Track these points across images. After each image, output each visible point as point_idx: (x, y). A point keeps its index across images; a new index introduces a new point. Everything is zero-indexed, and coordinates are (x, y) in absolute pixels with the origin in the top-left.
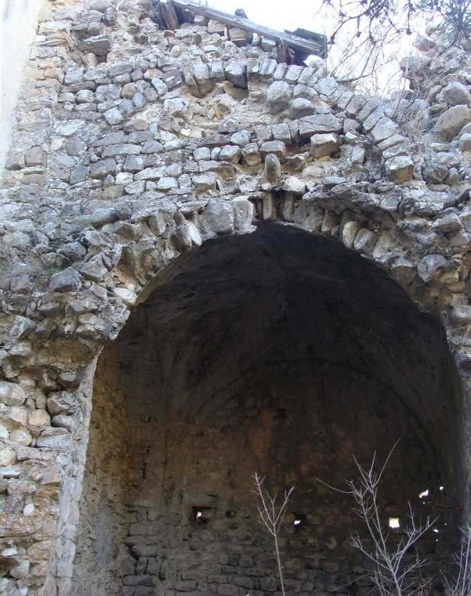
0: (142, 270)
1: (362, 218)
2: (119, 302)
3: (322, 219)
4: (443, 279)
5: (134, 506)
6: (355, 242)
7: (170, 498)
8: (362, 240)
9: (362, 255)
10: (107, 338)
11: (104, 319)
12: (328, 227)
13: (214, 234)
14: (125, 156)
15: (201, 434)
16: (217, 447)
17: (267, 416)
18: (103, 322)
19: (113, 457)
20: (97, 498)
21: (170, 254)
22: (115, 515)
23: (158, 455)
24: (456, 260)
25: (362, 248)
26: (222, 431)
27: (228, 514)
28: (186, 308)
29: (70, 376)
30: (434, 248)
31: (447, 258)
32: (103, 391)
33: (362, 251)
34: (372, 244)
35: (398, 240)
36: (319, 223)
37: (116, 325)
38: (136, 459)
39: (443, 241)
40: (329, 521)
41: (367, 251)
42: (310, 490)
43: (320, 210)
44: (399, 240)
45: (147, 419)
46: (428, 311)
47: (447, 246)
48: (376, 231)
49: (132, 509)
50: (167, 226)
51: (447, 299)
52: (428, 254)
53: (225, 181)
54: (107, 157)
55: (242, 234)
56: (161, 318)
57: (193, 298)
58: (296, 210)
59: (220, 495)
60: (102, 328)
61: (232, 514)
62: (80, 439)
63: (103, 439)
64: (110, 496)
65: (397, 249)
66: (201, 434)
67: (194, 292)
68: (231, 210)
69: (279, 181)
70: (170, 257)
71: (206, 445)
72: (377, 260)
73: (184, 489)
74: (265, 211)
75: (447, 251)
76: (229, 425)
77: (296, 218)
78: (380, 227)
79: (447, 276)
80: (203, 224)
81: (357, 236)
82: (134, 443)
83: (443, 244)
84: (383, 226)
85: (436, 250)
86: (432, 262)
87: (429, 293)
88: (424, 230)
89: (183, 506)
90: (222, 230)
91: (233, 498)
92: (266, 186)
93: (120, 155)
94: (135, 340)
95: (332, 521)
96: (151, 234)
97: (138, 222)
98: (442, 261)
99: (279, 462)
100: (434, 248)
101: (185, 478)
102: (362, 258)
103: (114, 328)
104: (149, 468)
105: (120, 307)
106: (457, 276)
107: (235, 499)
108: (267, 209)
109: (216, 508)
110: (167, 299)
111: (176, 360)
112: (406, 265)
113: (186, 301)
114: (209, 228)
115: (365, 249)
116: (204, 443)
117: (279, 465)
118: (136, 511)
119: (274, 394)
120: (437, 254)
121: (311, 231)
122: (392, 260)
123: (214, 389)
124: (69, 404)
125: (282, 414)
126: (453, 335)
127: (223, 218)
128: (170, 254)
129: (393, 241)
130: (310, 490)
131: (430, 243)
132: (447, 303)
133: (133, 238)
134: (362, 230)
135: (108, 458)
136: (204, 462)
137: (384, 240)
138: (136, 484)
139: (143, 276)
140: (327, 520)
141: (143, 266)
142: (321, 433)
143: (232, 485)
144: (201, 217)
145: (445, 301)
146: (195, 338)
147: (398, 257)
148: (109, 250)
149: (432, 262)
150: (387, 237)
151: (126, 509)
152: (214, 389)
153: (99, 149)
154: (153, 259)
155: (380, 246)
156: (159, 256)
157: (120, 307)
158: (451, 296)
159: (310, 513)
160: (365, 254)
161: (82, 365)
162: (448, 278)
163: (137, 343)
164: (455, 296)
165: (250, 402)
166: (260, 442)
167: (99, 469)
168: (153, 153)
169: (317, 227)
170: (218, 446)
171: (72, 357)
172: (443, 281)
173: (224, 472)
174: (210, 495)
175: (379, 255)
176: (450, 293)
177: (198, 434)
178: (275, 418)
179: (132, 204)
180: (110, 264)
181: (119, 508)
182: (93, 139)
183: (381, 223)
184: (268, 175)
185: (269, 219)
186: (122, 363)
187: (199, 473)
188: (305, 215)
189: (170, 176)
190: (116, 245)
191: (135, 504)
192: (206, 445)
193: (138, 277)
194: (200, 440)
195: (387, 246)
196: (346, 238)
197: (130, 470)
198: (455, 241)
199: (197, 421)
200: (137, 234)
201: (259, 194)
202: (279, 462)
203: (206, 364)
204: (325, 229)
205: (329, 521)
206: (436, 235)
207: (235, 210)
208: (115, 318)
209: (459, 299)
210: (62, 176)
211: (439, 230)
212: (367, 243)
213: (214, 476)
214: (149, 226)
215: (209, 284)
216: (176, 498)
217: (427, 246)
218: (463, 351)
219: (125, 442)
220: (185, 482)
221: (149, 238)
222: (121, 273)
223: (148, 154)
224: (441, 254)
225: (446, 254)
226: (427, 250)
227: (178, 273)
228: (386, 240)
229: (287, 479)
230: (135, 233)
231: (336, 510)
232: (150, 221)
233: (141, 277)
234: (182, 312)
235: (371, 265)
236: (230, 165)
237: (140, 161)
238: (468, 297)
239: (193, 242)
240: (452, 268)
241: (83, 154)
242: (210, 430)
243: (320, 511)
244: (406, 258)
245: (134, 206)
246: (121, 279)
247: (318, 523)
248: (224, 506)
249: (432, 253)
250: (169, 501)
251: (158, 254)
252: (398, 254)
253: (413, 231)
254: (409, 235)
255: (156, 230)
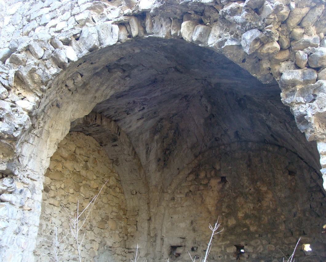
0: (36, 85)
1: (196, 17)
2: (20, 110)
3: (170, 26)
4: (265, 50)
5: (131, 249)
6: (193, 36)
7: (155, 241)
8: (196, 33)
9: (200, 45)
10: (12, 136)
11: (8, 123)
12: (175, 30)
13: (87, 51)
14: (41, 16)
15: (173, 199)
16: (183, 207)
17: (214, 183)
18: (7, 125)
19: (110, 219)
20: (96, 246)
21: (54, 70)
22: (116, 255)
23: (144, 216)
24: (267, 30)
25: (197, 39)
26: (186, 195)
27: (193, 249)
28: (142, 118)
29: (3, 167)
30: (248, 24)
31: (261, 31)
32: (95, 177)
33: (198, 41)
34: (206, 34)
35: (225, 27)
36: (168, 30)
37: (17, 126)
38: (131, 219)
39: (255, 17)
40: (260, 249)
41: (203, 41)
42: (245, 229)
43: (168, 20)
44: (226, 27)
45: (135, 193)
46: (268, 82)
47: (260, 20)
48: (208, 24)
49: (130, 251)
50: (45, 50)
51: (277, 67)
52: (246, 31)
53: (100, 16)
54: (32, 20)
55: (105, 47)
56: (130, 127)
57: (145, 111)
58: (154, 24)
59: (187, 237)
60: (6, 129)
61: (195, 249)
62: (31, 209)
63: (98, 208)
64: (109, 243)
65: (226, 35)
66: (173, 199)
67: (145, 106)
68: (95, 31)
69: (135, 5)
70: (54, 73)
71: (176, 206)
72: (210, 46)
73: (164, 235)
74: (132, 30)
75: (260, 25)
76: (190, 191)
77: (155, 30)
78: (210, 20)
79: (267, 46)
80: (81, 47)
81: (194, 31)
82: (129, 209)
83: (255, 19)
84: (211, 18)
85: (250, 25)
86: (248, 36)
87: (262, 65)
88: (239, 11)
89: (164, 246)
90: (90, 47)
91: (195, 238)
92: (128, 11)
93: (38, 17)
94: (115, 143)
95: (262, 249)
96: (33, 58)
97: (22, 51)
98: (256, 33)
99: (224, 212)
100: (248, 24)
101: (165, 228)
102: (201, 47)
103: (17, 129)
104: (139, 224)
105: (22, 113)
106: (276, 45)
107: (196, 239)
108: (134, 29)
109: (185, 246)
110: (128, 114)
111: (148, 152)
112: (231, 44)
113: (141, 113)
114: (84, 48)
115: (200, 40)
116: (175, 205)
117: (223, 214)
118: (133, 252)
119: (218, 167)
120: (252, 28)
121: (164, 36)
122: (221, 43)
123: (178, 169)
124: (6, 186)
125: (223, 180)
126: (287, 96)
127: (90, 38)
128: (54, 70)
129: (222, 28)
130: (245, 229)
131: (244, 20)
132: (277, 70)
133: (21, 64)
134: (197, 26)
135: (104, 220)
136: (175, 217)
137: (215, 30)
138: (132, 235)
139: (38, 90)
140: (258, 249)
141: (35, 83)
142: (250, 189)
143: (194, 230)
144: (78, 42)
145: (275, 70)
146: (156, 137)
147: (226, 40)
148: (6, 75)
149: (248, 36)
150: (217, 27)
151: (126, 250)
152: (178, 169)
153: (28, 17)
154: (39, 76)
155: (212, 35)
156: (43, 73)
157: (22, 113)
158: (280, 65)
159: (246, 245)
160: (201, 43)
161: (10, 158)
162: (269, 48)
163: (116, 145)
164: (283, 64)
165: (202, 175)
166: (211, 200)
167: (96, 228)
168: (55, 9)
169: (167, 33)
170: (184, 206)
171: (3, 154)
172: (265, 52)
173: (188, 222)
174: (181, 238)
175: (212, 42)
176: (278, 62)
177: (171, 199)
178: (219, 183)
179: (17, 40)
180: (7, 85)
181: (119, 250)
182: (25, 12)
183: (210, 17)
184: (127, 4)
185: (137, 36)
186: (113, 159)
187: (173, 224)
188: (160, 26)
189: (64, 21)
190: (10, 70)
191: (132, 247)
192: (176, 206)
193: (35, 91)
194: (172, 203)
195: (217, 34)
196: (183, 33)
197: (128, 226)
198: (265, 14)
199: (170, 191)
200: (23, 60)
201: (122, 18)
202: (224, 212)
203: (167, 153)
204: (173, 32)
205: (260, 249)
206: (246, 12)
207: (98, 32)
208: (16, 122)
209: (286, 66)
210: (8, 39)
211: (248, 8)
212: (201, 35)
213: (183, 225)
214: (31, 53)
215: (151, 99)
216: (159, 241)
217: (243, 24)
218: (296, 108)
219: (120, 208)
220: (165, 231)
221: (32, 62)
222: (23, 90)
223: (53, 11)
224: (256, 28)
225: (260, 27)
226: (246, 27)
227: (112, 92)
228: (217, 29)
229: (229, 223)
230: (21, 59)
231: (264, 242)
232: (30, 48)
233: (37, 90)
234: (141, 121)
235: (210, 51)
236: (100, 3)
237: (48, 17)
238: (293, 63)
239: (69, 61)
240: (269, 38)
241: (20, 23)
242: (178, 196)
243: (252, 243)
244: (232, 40)
245: (19, 41)
246: (24, 94)
247: (252, 251)
248: (189, 244)
249: (249, 30)
250: (154, 244)
251: (42, 72)
252: (226, 38)
253: (231, 15)
254: (229, 19)
255: (35, 55)
